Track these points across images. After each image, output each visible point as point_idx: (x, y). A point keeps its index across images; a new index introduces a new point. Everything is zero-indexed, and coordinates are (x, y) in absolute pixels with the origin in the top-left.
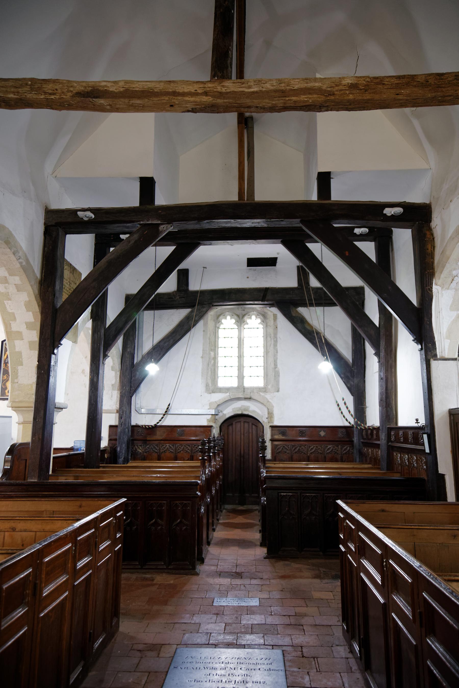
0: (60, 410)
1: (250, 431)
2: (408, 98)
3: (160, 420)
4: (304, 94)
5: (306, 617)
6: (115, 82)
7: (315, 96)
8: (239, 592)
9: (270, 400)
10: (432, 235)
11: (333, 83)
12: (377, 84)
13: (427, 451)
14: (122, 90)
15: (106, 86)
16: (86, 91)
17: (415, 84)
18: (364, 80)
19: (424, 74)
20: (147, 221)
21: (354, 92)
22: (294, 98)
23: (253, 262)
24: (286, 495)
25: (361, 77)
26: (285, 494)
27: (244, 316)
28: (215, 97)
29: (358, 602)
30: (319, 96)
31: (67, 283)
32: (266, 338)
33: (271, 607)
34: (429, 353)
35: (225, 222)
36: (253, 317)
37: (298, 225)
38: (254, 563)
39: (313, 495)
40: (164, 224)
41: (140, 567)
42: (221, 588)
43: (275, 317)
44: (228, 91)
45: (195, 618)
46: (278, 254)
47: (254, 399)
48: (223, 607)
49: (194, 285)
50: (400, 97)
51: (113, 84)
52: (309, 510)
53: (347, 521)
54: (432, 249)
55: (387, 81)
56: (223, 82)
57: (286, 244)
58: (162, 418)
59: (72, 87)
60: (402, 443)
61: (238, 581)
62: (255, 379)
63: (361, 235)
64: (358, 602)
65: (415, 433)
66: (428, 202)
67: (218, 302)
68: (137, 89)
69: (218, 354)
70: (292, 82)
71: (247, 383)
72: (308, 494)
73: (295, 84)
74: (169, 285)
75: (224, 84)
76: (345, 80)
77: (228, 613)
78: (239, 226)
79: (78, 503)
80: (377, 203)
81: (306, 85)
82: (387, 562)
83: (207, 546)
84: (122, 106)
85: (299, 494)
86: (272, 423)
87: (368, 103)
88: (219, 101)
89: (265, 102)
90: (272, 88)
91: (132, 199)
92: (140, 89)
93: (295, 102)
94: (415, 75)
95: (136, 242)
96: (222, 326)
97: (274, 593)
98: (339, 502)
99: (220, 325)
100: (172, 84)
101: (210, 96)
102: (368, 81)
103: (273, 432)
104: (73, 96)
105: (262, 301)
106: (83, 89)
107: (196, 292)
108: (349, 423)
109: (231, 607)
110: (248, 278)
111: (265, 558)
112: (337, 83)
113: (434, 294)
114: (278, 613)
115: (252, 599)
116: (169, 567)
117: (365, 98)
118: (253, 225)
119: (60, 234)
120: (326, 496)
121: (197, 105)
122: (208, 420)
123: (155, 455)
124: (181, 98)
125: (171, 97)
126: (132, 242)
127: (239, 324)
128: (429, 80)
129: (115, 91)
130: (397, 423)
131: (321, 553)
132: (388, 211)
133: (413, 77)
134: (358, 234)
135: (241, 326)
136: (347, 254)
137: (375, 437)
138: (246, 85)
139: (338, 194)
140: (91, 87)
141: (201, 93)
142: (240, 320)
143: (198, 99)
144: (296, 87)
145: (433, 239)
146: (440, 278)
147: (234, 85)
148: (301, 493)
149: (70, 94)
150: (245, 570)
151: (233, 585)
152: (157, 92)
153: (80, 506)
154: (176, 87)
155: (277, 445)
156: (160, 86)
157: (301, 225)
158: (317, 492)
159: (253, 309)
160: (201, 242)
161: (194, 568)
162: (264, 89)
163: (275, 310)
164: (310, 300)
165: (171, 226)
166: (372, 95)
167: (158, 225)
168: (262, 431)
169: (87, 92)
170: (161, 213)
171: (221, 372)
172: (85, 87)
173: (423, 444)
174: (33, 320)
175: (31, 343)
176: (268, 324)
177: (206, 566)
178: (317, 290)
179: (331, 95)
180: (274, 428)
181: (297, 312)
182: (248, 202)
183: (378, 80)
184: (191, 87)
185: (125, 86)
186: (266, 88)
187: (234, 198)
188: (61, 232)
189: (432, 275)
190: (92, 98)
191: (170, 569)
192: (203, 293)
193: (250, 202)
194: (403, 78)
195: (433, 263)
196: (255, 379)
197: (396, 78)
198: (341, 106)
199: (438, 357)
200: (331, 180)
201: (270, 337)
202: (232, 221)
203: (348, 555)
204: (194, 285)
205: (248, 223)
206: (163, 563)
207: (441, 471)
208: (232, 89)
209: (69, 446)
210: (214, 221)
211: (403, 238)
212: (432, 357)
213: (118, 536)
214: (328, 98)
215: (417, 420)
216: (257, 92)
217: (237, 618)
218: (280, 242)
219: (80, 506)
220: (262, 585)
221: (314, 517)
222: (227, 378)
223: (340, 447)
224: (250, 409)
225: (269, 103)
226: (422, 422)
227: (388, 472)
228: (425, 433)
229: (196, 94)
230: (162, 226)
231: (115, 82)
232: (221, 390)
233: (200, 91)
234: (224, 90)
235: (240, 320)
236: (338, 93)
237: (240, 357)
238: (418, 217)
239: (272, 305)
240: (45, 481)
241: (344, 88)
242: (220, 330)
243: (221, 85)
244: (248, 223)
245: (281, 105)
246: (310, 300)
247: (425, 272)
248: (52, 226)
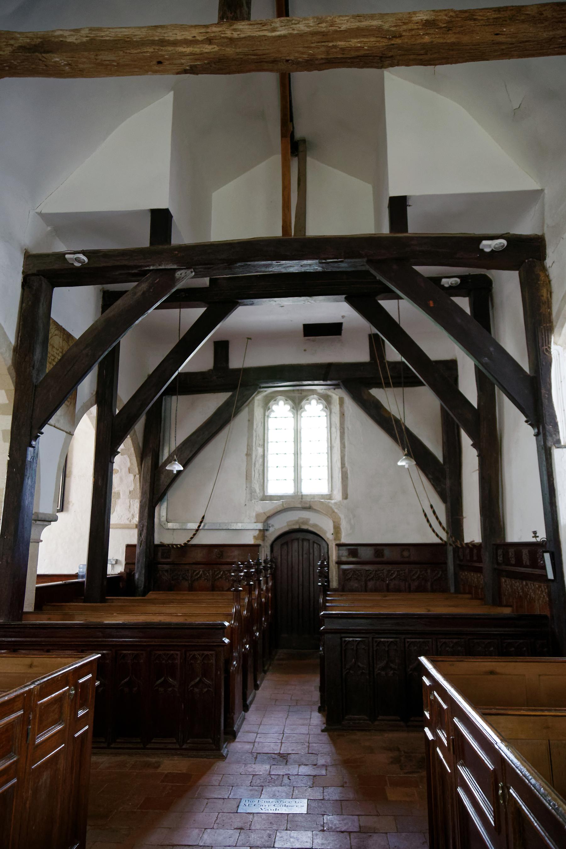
0: (46, 523)
1: (311, 551)
2: (514, 40)
3: (192, 538)
4: (356, 37)
5: (375, 835)
6: (77, 30)
7: (373, 39)
8: (280, 788)
9: (336, 510)
10: (548, 276)
11: (399, 20)
12: (466, 19)
13: (551, 576)
14: (85, 39)
15: (62, 36)
16: (33, 43)
17: (523, 18)
18: (446, 15)
19: (536, 5)
20: (159, 266)
21: (431, 31)
22: (341, 44)
23: (313, 330)
24: (353, 640)
25: (440, 11)
26: (351, 639)
27: (301, 400)
28: (222, 46)
29: (454, 831)
30: (379, 39)
31: (58, 354)
32: (331, 428)
33: (324, 815)
34: (549, 438)
35: (264, 265)
36: (314, 402)
37: (363, 268)
38: (307, 740)
39: (391, 640)
40: (182, 269)
41: (142, 746)
42: (254, 781)
44: (242, 36)
45: (205, 836)
46: (343, 317)
47: (315, 510)
48: (251, 816)
49: (236, 362)
50: (501, 39)
51: (72, 33)
52: (385, 662)
53: (435, 693)
54: (549, 296)
55: (480, 16)
56: (234, 23)
57: (351, 300)
58: (194, 535)
59: (12, 38)
60: (514, 565)
61: (281, 770)
63: (451, 287)
64: (454, 831)
65: (534, 549)
66: (540, 233)
67: (267, 383)
68: (108, 38)
69: (267, 451)
70: (338, 21)
72: (382, 640)
73: (342, 24)
74: (198, 360)
75: (235, 26)
76: (417, 15)
77: (258, 827)
78: (284, 271)
79: (27, 661)
80: (469, 236)
81: (358, 24)
83: (243, 712)
84: (86, 66)
85: (370, 639)
86: (340, 540)
87: (453, 50)
88: (230, 51)
89: (298, 52)
90: (309, 30)
91: (142, 238)
92: (111, 39)
93: (343, 49)
94: (523, 6)
95: (144, 293)
96: (272, 415)
97: (331, 790)
98: (423, 659)
99: (270, 413)
100: (159, 30)
101: (215, 44)
102: (451, 16)
103: (341, 552)
104: (13, 52)
105: (324, 380)
106: (28, 41)
107: (238, 370)
108: (441, 539)
109: (264, 816)
110: (305, 350)
111: (323, 731)
112: (405, 19)
113: (553, 356)
114: (334, 827)
115: (297, 800)
116: (184, 747)
117: (448, 41)
118: (303, 270)
119: (44, 286)
120: (408, 642)
121: (197, 60)
122: (254, 537)
123: (186, 584)
124: (172, 48)
125: (157, 48)
126: (139, 294)
127: (295, 412)
128: (544, 12)
129: (75, 41)
130: (504, 538)
131: (402, 723)
132: (487, 245)
133: (519, 9)
134: (447, 286)
135: (297, 414)
136: (431, 304)
137: (475, 558)
138: (269, 27)
139: (415, 225)
140: (41, 38)
141: (202, 41)
142: (297, 404)
143: (197, 49)
144: (343, 27)
145: (550, 281)
146: (560, 334)
147: (251, 27)
148: (373, 638)
149: (10, 49)
150: (293, 750)
151: (273, 777)
152: (137, 42)
153: (31, 666)
154: (165, 33)
155: (345, 571)
156: (141, 32)
157: (367, 267)
158: (394, 636)
159: (313, 392)
160: (240, 301)
161: (219, 748)
162: (296, 32)
164: (386, 378)
165: (192, 272)
166: (457, 36)
167: (175, 270)
168: (326, 550)
169: (35, 45)
170: (178, 254)
171: (272, 474)
172: (32, 39)
173: (544, 567)
174: (7, 402)
175: (4, 432)
176: (333, 411)
177: (238, 744)
178: (395, 365)
179: (395, 37)
180: (341, 548)
181: (370, 394)
182: (295, 237)
183: (467, 15)
184: (187, 33)
185: (90, 35)
186: (298, 30)
187: (278, 233)
188: (45, 284)
189: (550, 330)
190: (41, 53)
191: (185, 749)
192: (246, 371)
193: (298, 237)
194: (503, 11)
195: (550, 314)
197: (495, 11)
198: (412, 57)
199: (562, 443)
200: (408, 208)
201: (336, 428)
202: (274, 262)
203: (438, 749)
204: (236, 362)
205: (294, 266)
206: (175, 741)
208: (249, 34)
209: (73, 572)
210: (249, 263)
211: (508, 286)
212: (554, 444)
213: (81, 713)
214: (393, 42)
215: (535, 533)
216: (284, 36)
217: (269, 836)
218: (344, 299)
219: (31, 666)
220: (315, 776)
221: (392, 672)
222: (279, 484)
223: (429, 571)
224: (311, 522)
225: (303, 53)
226: (542, 535)
228: (546, 552)
229: (193, 42)
230: (179, 273)
231: (77, 31)
232: (271, 498)
233: (200, 38)
234: (235, 35)
235: (297, 404)
236: (408, 34)
237: (297, 454)
238: (526, 254)
239: (337, 386)
240: (19, 623)
241: (416, 27)
242: (270, 420)
243: (232, 27)
244: (294, 266)
245: (323, 57)
246: (386, 378)
247: (538, 329)
248: (33, 275)
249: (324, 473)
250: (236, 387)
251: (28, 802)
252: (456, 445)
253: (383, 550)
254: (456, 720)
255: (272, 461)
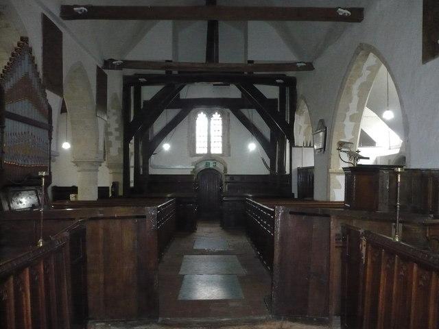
43: (229, 113)
62: (217, 149)
71: (213, 151)
82: (143, 108)
107: (184, 99)
142: (209, 116)
163: (228, 110)
171: (198, 145)
189: (295, 111)
196: (217, 149)
207: (293, 192)
222: (201, 149)
227: (290, 74)
235: (209, 116)
249: (220, 145)
250: (188, 108)
251: (365, 316)
252: (278, 137)
253: (145, 102)
254: (132, 185)
255: (198, 139)
